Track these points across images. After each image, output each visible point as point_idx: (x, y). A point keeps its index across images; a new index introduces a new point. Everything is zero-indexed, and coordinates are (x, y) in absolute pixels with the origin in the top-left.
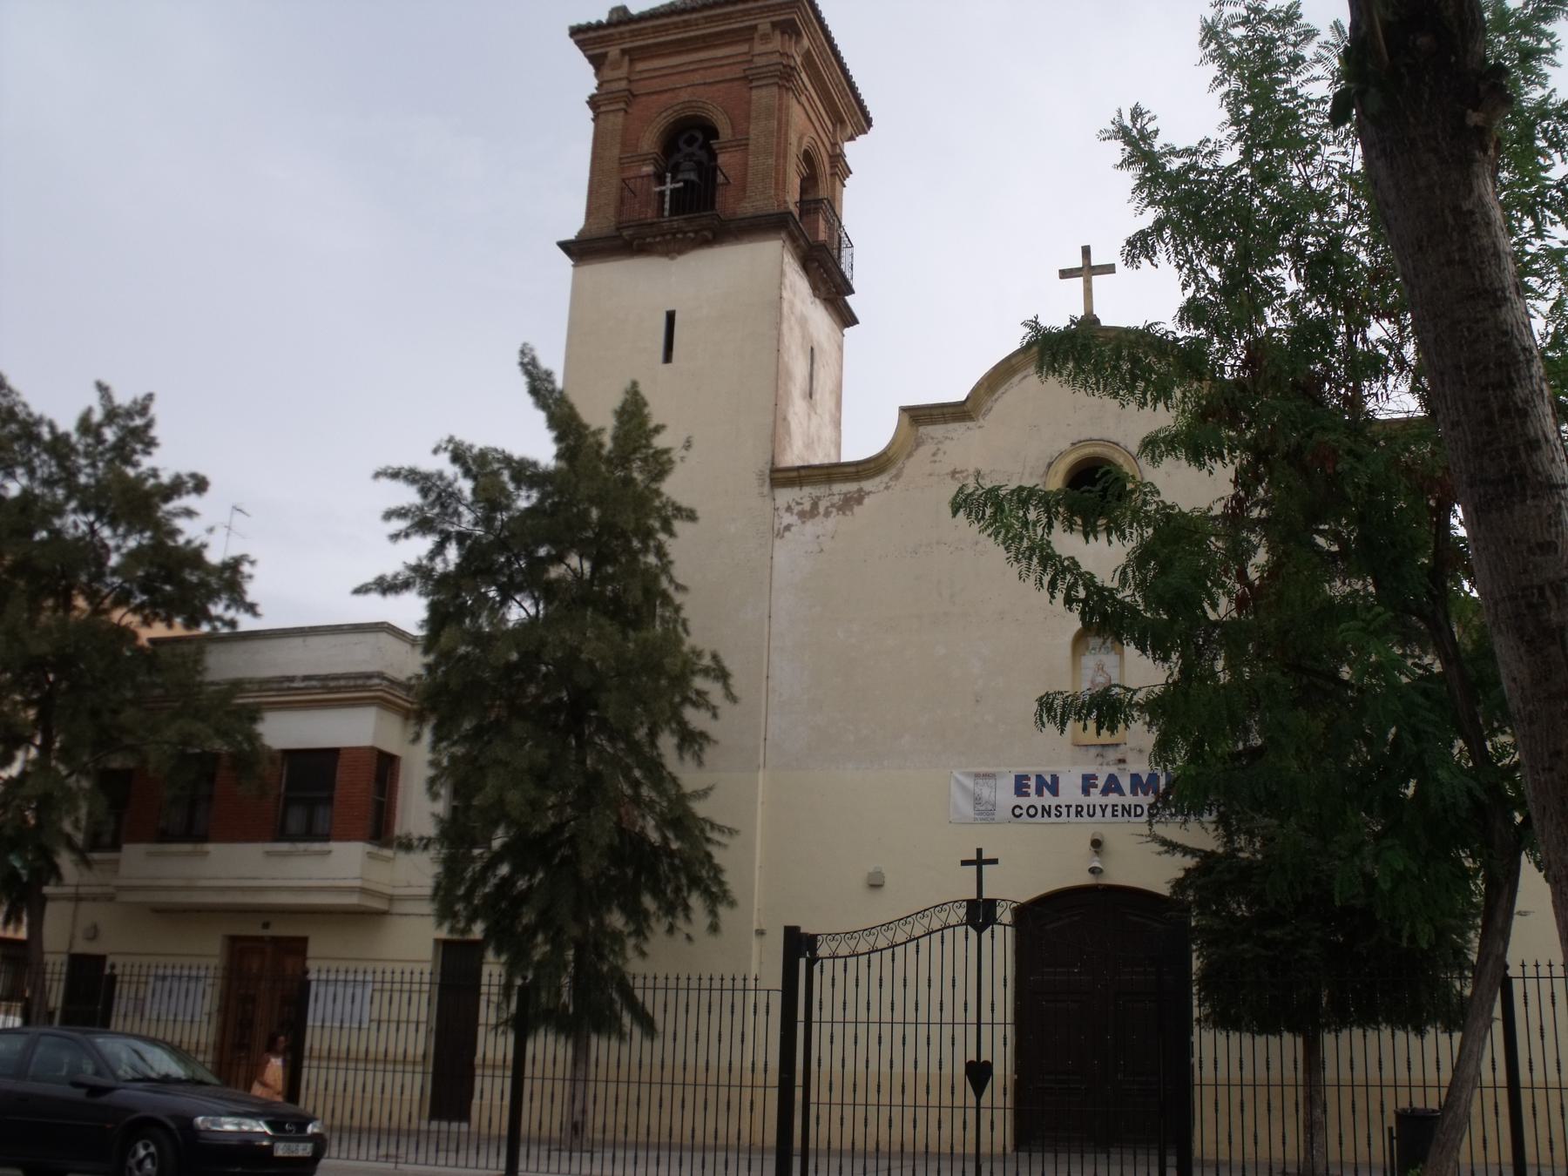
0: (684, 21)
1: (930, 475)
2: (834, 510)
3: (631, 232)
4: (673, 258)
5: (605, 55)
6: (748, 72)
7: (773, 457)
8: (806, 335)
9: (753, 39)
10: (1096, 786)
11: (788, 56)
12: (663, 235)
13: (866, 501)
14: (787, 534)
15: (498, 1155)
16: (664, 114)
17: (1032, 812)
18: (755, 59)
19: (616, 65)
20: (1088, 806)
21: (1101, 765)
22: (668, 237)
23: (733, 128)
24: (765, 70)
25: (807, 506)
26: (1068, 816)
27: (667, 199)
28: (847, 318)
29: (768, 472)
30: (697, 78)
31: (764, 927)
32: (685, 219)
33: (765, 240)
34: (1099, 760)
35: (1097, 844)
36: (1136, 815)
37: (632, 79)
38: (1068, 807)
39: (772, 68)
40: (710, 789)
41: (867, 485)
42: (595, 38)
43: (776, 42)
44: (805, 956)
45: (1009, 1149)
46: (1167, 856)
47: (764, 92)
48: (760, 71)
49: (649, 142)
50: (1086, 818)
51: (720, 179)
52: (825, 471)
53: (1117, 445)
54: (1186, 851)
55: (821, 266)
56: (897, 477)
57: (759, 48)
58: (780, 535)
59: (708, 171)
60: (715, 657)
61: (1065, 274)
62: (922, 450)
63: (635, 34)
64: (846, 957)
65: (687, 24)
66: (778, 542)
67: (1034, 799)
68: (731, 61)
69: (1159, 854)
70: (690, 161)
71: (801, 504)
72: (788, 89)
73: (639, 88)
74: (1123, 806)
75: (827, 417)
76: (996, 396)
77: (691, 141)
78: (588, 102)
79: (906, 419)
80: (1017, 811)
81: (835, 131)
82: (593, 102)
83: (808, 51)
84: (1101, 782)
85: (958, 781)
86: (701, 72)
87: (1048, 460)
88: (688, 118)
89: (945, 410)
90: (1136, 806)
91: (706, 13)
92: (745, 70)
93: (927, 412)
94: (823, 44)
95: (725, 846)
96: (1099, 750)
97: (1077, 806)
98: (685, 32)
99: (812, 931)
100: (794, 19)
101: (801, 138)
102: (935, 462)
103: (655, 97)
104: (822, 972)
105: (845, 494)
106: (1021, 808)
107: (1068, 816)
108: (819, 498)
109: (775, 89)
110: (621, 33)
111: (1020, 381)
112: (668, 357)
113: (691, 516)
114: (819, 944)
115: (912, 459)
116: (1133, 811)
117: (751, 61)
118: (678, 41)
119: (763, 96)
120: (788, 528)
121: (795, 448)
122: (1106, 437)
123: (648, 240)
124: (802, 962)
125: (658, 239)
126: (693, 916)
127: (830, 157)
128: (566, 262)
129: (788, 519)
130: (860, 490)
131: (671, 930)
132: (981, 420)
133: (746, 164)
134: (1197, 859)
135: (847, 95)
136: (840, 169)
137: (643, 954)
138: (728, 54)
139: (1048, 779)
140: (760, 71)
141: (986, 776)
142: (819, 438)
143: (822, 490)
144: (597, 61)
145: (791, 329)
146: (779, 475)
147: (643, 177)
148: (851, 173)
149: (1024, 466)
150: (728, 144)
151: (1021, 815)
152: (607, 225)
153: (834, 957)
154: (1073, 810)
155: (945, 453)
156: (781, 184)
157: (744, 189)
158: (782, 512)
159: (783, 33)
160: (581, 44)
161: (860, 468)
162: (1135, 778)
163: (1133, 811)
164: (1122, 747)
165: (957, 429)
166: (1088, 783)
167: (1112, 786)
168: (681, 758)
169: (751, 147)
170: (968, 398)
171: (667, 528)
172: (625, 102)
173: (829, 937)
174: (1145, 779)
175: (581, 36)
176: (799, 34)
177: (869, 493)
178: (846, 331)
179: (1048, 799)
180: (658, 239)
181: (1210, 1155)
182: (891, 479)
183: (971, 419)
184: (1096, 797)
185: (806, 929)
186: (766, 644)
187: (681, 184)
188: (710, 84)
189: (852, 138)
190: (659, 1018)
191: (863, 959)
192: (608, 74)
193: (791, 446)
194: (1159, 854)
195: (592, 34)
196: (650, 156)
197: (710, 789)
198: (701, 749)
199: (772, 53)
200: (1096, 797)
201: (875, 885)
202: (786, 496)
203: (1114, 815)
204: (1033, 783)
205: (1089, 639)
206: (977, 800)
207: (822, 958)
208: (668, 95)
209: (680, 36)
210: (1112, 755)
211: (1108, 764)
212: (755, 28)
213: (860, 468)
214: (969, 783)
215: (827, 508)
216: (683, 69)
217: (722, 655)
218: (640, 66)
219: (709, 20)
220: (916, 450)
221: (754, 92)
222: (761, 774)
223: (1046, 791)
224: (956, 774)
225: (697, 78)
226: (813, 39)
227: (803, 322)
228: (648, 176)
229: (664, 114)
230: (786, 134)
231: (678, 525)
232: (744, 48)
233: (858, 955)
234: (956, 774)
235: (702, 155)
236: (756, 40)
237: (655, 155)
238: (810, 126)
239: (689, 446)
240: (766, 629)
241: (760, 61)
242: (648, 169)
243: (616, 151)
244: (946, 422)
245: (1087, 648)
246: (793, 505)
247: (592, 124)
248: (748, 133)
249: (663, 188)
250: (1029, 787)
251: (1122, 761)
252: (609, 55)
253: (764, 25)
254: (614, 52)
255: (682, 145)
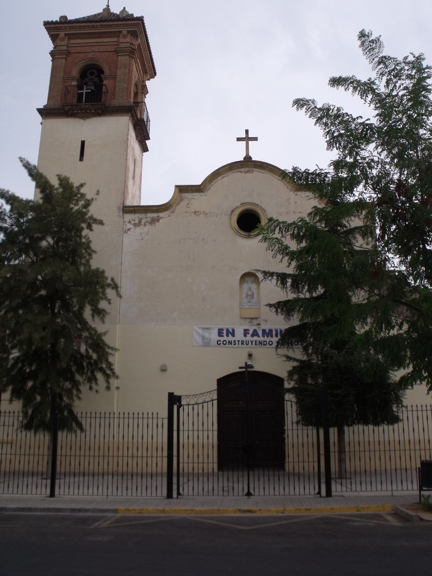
0: (92, 26)
1: (186, 212)
2: (148, 224)
3: (68, 108)
4: (84, 120)
5: (58, 35)
6: (117, 49)
7: (124, 201)
8: (134, 155)
9: (119, 36)
10: (249, 334)
11: (133, 45)
12: (81, 110)
13: (161, 221)
14: (128, 232)
15: (46, 488)
16: (82, 62)
17: (225, 343)
18: (120, 44)
19: (62, 40)
20: (246, 341)
21: (251, 325)
22: (84, 111)
23: (110, 71)
24: (124, 49)
25: (137, 222)
26: (239, 344)
27: (84, 96)
28: (145, 149)
29: (122, 207)
30: (95, 49)
31: (119, 386)
32: (91, 105)
33: (122, 116)
34: (250, 324)
35: (250, 355)
36: (264, 345)
37: (69, 46)
38: (239, 341)
39: (127, 49)
40: (107, 332)
41: (161, 215)
42: (54, 27)
43: (129, 39)
44: (176, 404)
45: (216, 470)
46: (288, 362)
47: (123, 58)
48: (122, 49)
49: (75, 72)
50: (245, 345)
51: (104, 89)
52: (145, 208)
53: (258, 205)
54: (295, 360)
55: (140, 128)
56: (173, 212)
57: (122, 40)
58: (126, 232)
59: (99, 86)
60: (112, 280)
61: (239, 139)
62: (182, 202)
63: (71, 28)
64: (193, 405)
65: (93, 27)
66: (125, 235)
67: (225, 338)
68: (110, 44)
69: (285, 361)
70: (92, 81)
71: (135, 220)
72: (132, 58)
73: (72, 50)
74: (259, 341)
75: (138, 186)
76: (213, 183)
77: (92, 74)
78: (50, 53)
79: (177, 190)
80: (219, 343)
81: (144, 76)
82: (52, 54)
83: (140, 44)
84: (251, 332)
85: (195, 330)
86: (97, 47)
87: (232, 210)
88: (92, 64)
89: (193, 188)
90: (264, 341)
91: (101, 24)
92: (116, 48)
93: (186, 188)
94: (145, 42)
95: (113, 355)
96: (250, 320)
97: (242, 341)
98: (92, 30)
99: (179, 394)
100: (136, 30)
101: (135, 78)
102: (188, 207)
103: (78, 54)
104: (183, 411)
105: (152, 218)
106: (220, 341)
107: (239, 344)
108: (142, 219)
109: (128, 57)
110: (65, 27)
111: (221, 179)
112: (81, 159)
113: (101, 223)
114: (182, 399)
115: (179, 206)
116: (263, 343)
117: (118, 45)
118: (89, 33)
119: (123, 59)
120: (129, 229)
121: (129, 198)
122: (254, 202)
123: (75, 111)
124: (175, 407)
125: (79, 112)
126: (98, 383)
127: (142, 86)
128: (39, 118)
129: (129, 226)
130: (158, 216)
131: (91, 388)
132: (206, 193)
133: (115, 85)
134: (298, 363)
135: (150, 62)
136: (144, 91)
137: (79, 398)
138: (109, 41)
139: (231, 331)
140: (122, 49)
141: (207, 329)
142: (135, 195)
143: (143, 215)
144: (54, 38)
145: (130, 152)
146: (127, 209)
147: (71, 86)
148: (148, 93)
149: (223, 212)
150: (108, 77)
151: (220, 344)
152: (57, 103)
153: (188, 405)
154: (240, 342)
155: (192, 204)
156: (128, 95)
157: (114, 95)
158: (127, 223)
159: (131, 35)
160: (48, 29)
161: (159, 208)
162: (264, 331)
163: (263, 343)
164: (259, 319)
165: (197, 195)
166: (246, 332)
167: (255, 333)
168: (93, 319)
169: (117, 79)
170: (202, 184)
171: (90, 227)
172: (66, 55)
173: (186, 397)
174: (267, 331)
175: (48, 26)
176: (137, 36)
177: (162, 218)
178: (144, 153)
179: (231, 338)
180: (79, 112)
181: (291, 471)
182: (170, 213)
183: (202, 192)
184: (249, 338)
185: (177, 393)
186: (120, 275)
187: (90, 91)
188: (101, 52)
189: (149, 80)
190: (83, 423)
191: (200, 406)
192: (59, 43)
193: (128, 197)
194: (285, 361)
195: (53, 26)
196: (76, 78)
197: (107, 332)
198: (104, 316)
199: (127, 43)
200: (249, 338)
201: (164, 370)
202: (128, 217)
203: (256, 345)
204: (225, 332)
205: (246, 278)
206: (203, 338)
207: (183, 405)
208: (84, 54)
209: (90, 31)
210: (255, 322)
211: (253, 325)
212: (121, 32)
213: (159, 208)
214: (200, 331)
215: (145, 223)
216: (90, 45)
217: (116, 280)
218: (72, 41)
219: (102, 26)
220: (181, 202)
221: (119, 57)
222: (118, 325)
223: (230, 335)
224: (195, 328)
225: (95, 49)
226: (142, 40)
227: (133, 149)
228: (74, 86)
229: (82, 62)
230: (131, 75)
231: (94, 226)
232: (116, 39)
233: (198, 404)
234: (195, 328)
235: (97, 80)
236: (121, 37)
237: (78, 78)
238: (137, 73)
239: (98, 194)
240: (120, 269)
241: (122, 45)
242: (74, 83)
243: (62, 74)
244: (192, 192)
245: (245, 281)
246: (131, 220)
247: (51, 63)
248: (116, 73)
249: (83, 91)
250: (223, 333)
251: (259, 324)
252: (60, 35)
253: (125, 32)
254: (62, 34)
255: (88, 74)
